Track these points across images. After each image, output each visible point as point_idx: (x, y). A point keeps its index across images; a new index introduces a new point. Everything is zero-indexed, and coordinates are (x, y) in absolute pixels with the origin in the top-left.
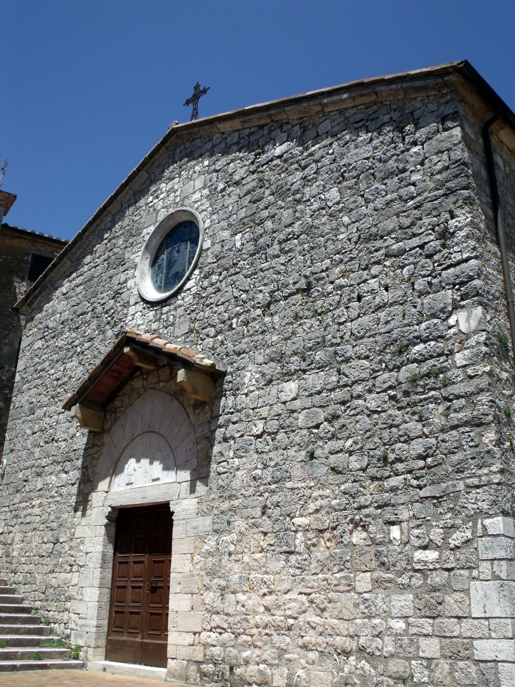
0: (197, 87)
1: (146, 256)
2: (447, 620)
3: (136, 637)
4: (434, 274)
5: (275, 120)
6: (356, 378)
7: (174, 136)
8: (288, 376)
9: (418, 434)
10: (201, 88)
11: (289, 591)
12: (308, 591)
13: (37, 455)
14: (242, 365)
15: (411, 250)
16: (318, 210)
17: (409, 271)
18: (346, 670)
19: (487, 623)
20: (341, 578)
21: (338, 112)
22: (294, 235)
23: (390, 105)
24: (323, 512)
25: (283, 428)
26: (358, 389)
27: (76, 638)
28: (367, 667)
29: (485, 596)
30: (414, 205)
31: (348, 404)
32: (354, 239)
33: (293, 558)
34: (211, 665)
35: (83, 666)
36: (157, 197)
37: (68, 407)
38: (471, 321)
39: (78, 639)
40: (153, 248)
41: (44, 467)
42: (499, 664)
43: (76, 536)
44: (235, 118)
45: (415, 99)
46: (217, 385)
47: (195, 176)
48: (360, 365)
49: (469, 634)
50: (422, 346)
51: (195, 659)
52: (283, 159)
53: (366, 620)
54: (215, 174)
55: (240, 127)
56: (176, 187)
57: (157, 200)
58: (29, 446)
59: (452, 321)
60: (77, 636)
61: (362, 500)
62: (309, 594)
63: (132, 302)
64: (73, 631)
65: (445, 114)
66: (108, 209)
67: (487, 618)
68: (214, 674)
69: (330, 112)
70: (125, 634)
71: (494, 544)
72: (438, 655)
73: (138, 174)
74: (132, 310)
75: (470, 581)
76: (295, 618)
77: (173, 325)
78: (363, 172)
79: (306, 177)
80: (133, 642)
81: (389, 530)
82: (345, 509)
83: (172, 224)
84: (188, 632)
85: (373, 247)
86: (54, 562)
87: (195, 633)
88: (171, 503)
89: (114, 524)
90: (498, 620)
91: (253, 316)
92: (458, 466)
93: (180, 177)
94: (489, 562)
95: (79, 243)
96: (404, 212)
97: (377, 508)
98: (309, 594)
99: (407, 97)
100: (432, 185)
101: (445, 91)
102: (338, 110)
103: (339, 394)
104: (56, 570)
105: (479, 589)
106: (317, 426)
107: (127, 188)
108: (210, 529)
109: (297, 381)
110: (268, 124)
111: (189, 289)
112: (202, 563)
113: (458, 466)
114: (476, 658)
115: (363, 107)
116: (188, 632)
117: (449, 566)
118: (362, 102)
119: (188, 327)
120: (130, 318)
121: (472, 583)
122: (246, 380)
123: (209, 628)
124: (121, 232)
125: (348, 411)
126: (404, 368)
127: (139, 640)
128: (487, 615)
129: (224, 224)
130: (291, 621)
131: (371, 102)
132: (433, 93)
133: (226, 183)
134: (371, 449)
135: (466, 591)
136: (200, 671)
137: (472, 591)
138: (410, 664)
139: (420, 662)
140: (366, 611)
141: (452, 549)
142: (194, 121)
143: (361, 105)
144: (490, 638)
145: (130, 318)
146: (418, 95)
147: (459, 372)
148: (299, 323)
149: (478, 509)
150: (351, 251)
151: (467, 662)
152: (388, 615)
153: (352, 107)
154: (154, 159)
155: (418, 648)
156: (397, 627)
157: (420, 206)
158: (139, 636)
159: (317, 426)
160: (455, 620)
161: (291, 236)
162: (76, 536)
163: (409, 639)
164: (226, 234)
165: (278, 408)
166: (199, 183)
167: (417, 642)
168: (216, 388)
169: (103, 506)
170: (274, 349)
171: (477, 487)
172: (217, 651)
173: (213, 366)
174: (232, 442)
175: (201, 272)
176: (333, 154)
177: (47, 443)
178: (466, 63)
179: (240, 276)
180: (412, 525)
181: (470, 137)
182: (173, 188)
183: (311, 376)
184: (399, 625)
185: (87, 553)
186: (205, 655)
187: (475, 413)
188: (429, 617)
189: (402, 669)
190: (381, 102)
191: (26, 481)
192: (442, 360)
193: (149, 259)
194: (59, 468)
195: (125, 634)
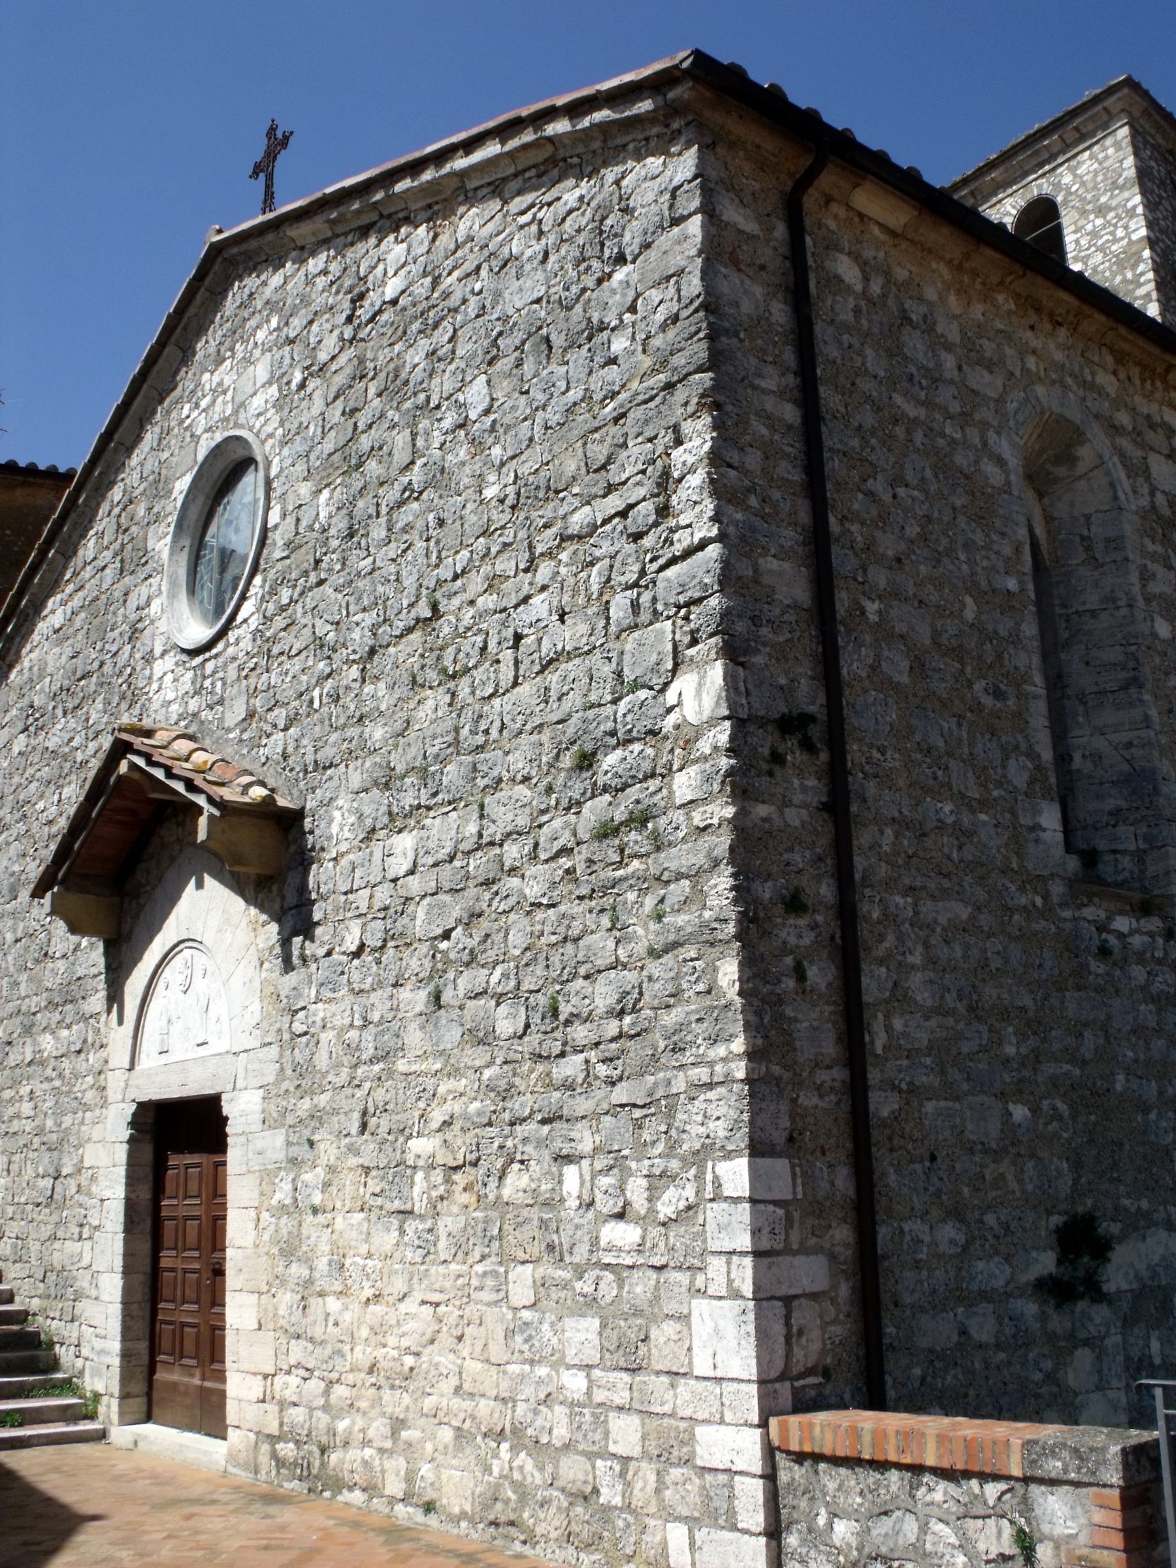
0: (272, 130)
1: (180, 545)
2: (653, 1377)
3: (192, 1376)
4: (643, 582)
5: (385, 213)
6: (508, 829)
7: (219, 260)
8: (396, 822)
9: (609, 961)
10: (279, 135)
11: (405, 1296)
12: (436, 1297)
13: (23, 989)
14: (328, 795)
15: (605, 522)
16: (453, 431)
17: (600, 573)
18: (496, 1471)
19: (718, 1391)
20: (485, 1274)
21: (490, 189)
22: (413, 491)
23: (580, 165)
24: (456, 1127)
25: (393, 938)
26: (512, 852)
27: (92, 1376)
28: (529, 1465)
29: (716, 1331)
30: (615, 414)
31: (495, 888)
32: (510, 501)
33: (412, 1226)
34: (291, 1445)
35: (102, 1435)
36: (197, 406)
37: (38, 893)
38: (704, 695)
39: (96, 1379)
40: (192, 524)
41: (34, 1014)
42: (737, 1478)
43: (86, 1164)
44: (315, 214)
45: (625, 146)
46: (290, 837)
47: (257, 353)
48: (515, 797)
49: (688, 1413)
50: (619, 753)
51: (267, 1431)
52: (398, 307)
53: (527, 1367)
54: (287, 348)
55: (329, 234)
56: (227, 382)
57: (196, 412)
58: (12, 969)
59: (671, 697)
60: (96, 1373)
61: (517, 1106)
62: (437, 1305)
63: (158, 652)
64: (88, 1363)
65: (675, 183)
66: (116, 437)
67: (719, 1380)
68: (295, 1464)
69: (476, 189)
70: (177, 1368)
71: (733, 1218)
72: (636, 1452)
73: (160, 353)
74: (159, 667)
75: (693, 1297)
76: (417, 1354)
77: (221, 702)
78: (530, 335)
79: (434, 353)
80: (187, 1385)
81: (561, 1175)
82: (490, 1124)
83: (220, 466)
84: (255, 1374)
85: (541, 517)
86: (55, 1218)
87: (266, 1377)
88: (224, 1097)
89: (149, 1137)
90: (735, 1385)
91: (344, 682)
92: (675, 1038)
93: (233, 357)
94: (724, 1259)
95: (73, 516)
96: (596, 430)
97: (544, 1122)
98: (437, 1305)
99: (610, 144)
100: (647, 362)
101: (675, 125)
102: (489, 184)
103: (478, 864)
104: (60, 1234)
105: (706, 1316)
106: (446, 935)
107: (145, 386)
108: (281, 1156)
109: (415, 832)
110: (375, 223)
111: (245, 621)
112: (272, 1227)
113: (675, 1038)
114: (699, 1463)
115: (533, 172)
116: (255, 1374)
117: (657, 1261)
118: (531, 163)
119: (244, 707)
120: (155, 686)
121: (694, 1302)
122: (335, 829)
123: (285, 1367)
124: (142, 488)
125: (495, 904)
126: (589, 803)
127: (197, 1381)
128: (719, 1374)
129: (301, 467)
130: (409, 1361)
131: (546, 160)
132: (655, 130)
133: (307, 368)
134: (531, 992)
135: (684, 1318)
136: (274, 1455)
137: (695, 1319)
138: (594, 1467)
139: (609, 1463)
140: (526, 1347)
141: (664, 1224)
142: (270, 216)
143: (529, 169)
144: (722, 1422)
145: (155, 686)
146: (629, 138)
147: (678, 816)
148: (417, 698)
149: (708, 1137)
150: (503, 527)
151: (685, 1471)
152: (559, 1362)
153: (516, 175)
154: (187, 315)
155: (607, 1433)
156: (574, 1388)
157: (623, 415)
158: (198, 1372)
159: (446, 935)
160: (665, 1379)
161: (407, 494)
162: (86, 1164)
163: (593, 1414)
164: (305, 489)
165: (383, 895)
166: (261, 371)
167: (606, 1421)
168: (288, 846)
169: (123, 1101)
170: (378, 760)
171: (710, 1086)
172: (297, 1415)
173: (269, 801)
174: (314, 966)
175: (265, 581)
176: (481, 292)
177: (37, 961)
178: (698, 54)
179: (327, 589)
180: (598, 1166)
181: (740, 232)
182: (220, 384)
183: (438, 821)
184: (575, 1383)
185: (102, 1200)
186: (281, 1425)
187: (707, 914)
188: (627, 1370)
189: (581, 1476)
190: (565, 160)
191: (9, 1043)
192: (652, 789)
193: (186, 550)
194: (56, 1017)
195: (177, 1368)
